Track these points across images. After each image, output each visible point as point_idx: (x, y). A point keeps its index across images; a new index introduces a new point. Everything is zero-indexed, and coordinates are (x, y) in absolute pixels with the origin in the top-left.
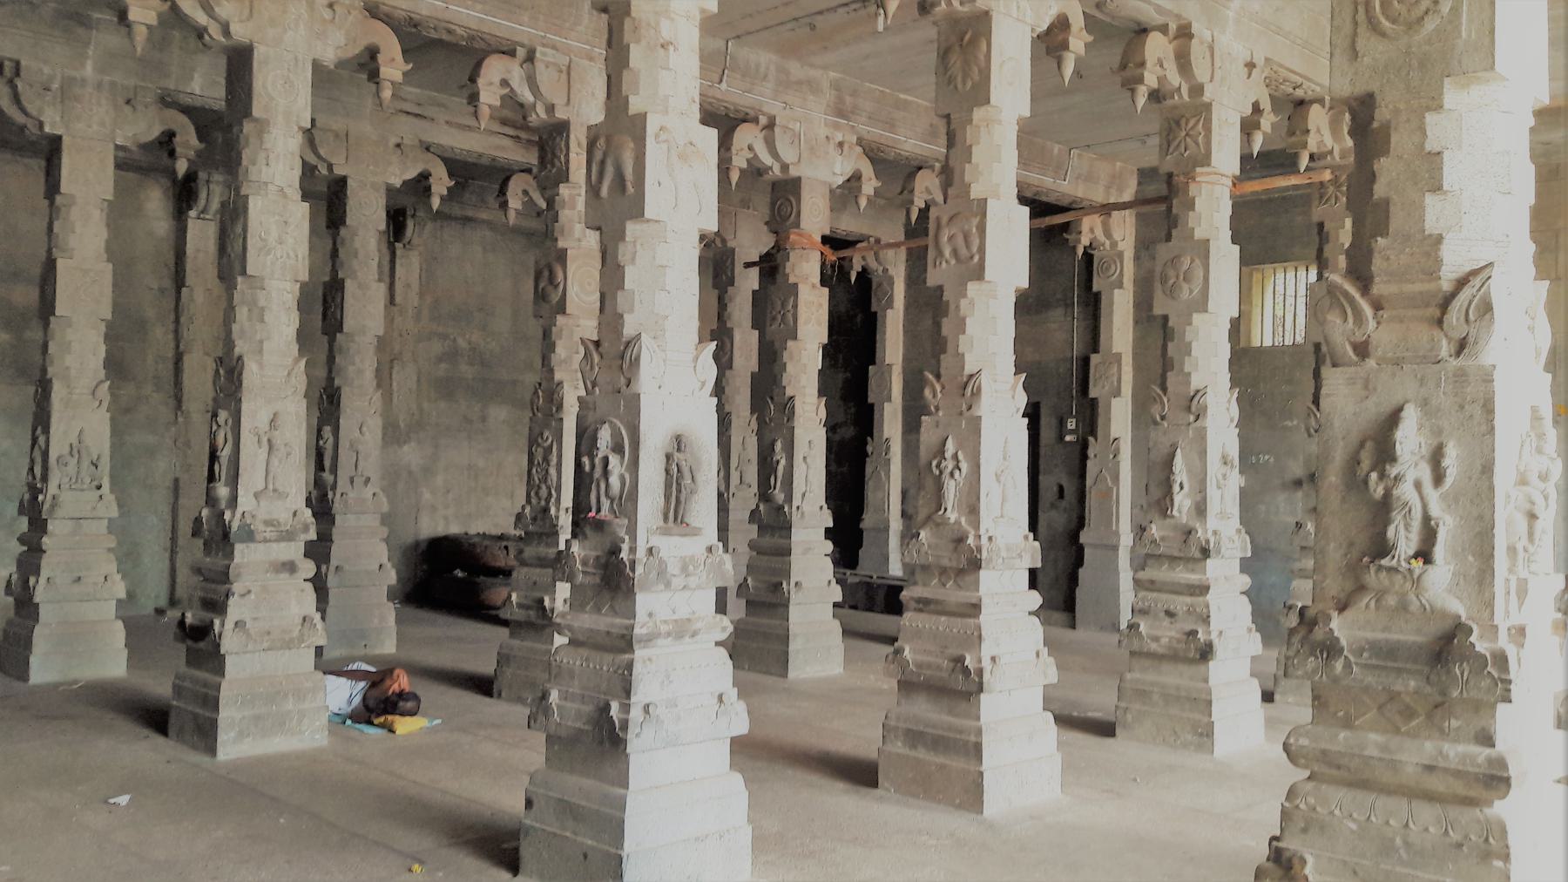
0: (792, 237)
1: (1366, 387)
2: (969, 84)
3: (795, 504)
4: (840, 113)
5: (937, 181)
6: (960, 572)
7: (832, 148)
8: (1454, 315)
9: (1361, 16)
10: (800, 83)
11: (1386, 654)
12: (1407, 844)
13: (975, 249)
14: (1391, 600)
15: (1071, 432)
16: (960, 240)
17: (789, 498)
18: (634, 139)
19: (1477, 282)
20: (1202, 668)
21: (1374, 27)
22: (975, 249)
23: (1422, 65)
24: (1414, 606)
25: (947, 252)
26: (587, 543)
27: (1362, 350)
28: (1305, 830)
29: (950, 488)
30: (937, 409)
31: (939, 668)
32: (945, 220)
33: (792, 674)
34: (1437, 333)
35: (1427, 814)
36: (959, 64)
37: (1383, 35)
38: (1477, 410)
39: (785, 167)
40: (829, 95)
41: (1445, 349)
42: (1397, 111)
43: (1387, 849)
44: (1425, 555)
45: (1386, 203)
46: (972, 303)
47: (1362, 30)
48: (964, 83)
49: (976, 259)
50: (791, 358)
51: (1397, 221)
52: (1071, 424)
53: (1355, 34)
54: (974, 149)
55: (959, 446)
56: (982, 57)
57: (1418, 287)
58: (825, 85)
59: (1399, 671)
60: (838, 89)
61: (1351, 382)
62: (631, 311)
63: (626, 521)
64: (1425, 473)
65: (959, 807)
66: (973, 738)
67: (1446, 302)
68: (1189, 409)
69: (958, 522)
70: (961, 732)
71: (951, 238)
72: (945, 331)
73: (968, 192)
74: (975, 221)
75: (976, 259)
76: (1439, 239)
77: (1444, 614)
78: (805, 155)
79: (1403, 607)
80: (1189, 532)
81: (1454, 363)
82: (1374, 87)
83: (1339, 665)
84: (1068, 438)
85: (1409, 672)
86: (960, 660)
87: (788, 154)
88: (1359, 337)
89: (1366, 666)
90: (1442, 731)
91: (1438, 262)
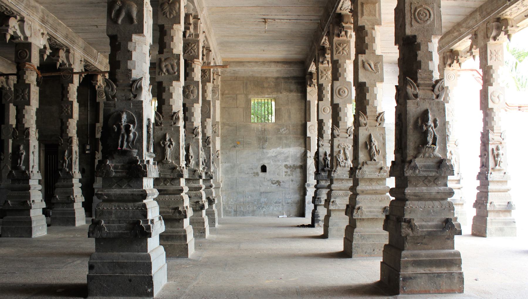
0: (27, 65)
1: (417, 105)
2: (172, 16)
3: (31, 170)
4: (43, 22)
5: (65, 54)
6: (173, 179)
7: (40, 34)
8: (436, 89)
9: (413, 17)
10: (33, 7)
11: (427, 168)
12: (433, 211)
13: (176, 70)
14: (427, 155)
15: (88, 150)
16: (170, 67)
17: (28, 168)
18: (137, 4)
19: (440, 82)
20: (200, 212)
21: (416, 21)
22: (176, 70)
23: (427, 31)
24: (432, 156)
25: (164, 70)
26: (114, 161)
27: (416, 96)
28: (410, 213)
29: (169, 151)
30: (161, 124)
31: (168, 212)
32: (163, 59)
33: (34, 236)
34: (433, 93)
35: (437, 203)
36: (168, 9)
37: (418, 22)
38: (442, 111)
39: (26, 38)
40: (41, 14)
41: (434, 97)
42: (422, 41)
43: (429, 213)
44: (434, 143)
45: (420, 62)
46: (174, 88)
47: (413, 20)
48: (170, 15)
49: (176, 74)
50: (27, 113)
51: (423, 66)
52: (88, 147)
53: (411, 21)
54: (174, 38)
55: (171, 136)
56: (177, 9)
57: (428, 82)
58: (40, 10)
59: (431, 171)
60: (43, 13)
61: (414, 103)
62: (134, 69)
63: (137, 151)
64: (433, 125)
65: (178, 257)
66: (183, 234)
67: (434, 86)
68: (193, 133)
69: (172, 163)
70: (177, 233)
71: (166, 66)
72: (164, 97)
73: (172, 52)
74: (176, 61)
75: (176, 74)
76: (432, 72)
77: (438, 157)
78: (33, 35)
79: (429, 157)
80: (195, 171)
81: (437, 100)
82: (416, 34)
83: (417, 171)
84: (87, 152)
85: (433, 171)
86: (177, 208)
87: (28, 33)
88: (415, 93)
89: (424, 171)
90: (437, 184)
91: (432, 77)
